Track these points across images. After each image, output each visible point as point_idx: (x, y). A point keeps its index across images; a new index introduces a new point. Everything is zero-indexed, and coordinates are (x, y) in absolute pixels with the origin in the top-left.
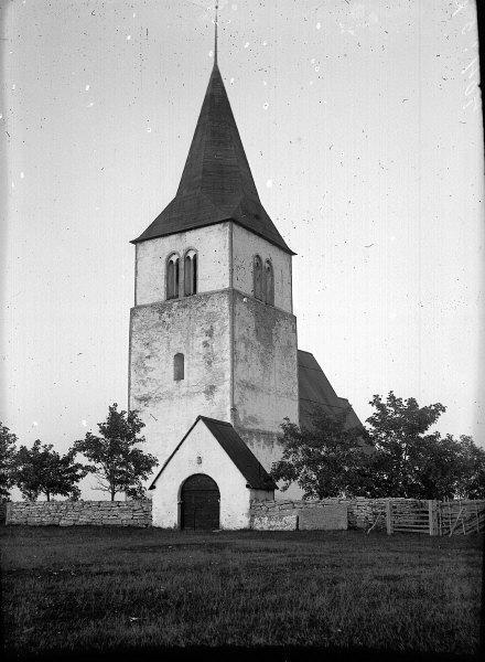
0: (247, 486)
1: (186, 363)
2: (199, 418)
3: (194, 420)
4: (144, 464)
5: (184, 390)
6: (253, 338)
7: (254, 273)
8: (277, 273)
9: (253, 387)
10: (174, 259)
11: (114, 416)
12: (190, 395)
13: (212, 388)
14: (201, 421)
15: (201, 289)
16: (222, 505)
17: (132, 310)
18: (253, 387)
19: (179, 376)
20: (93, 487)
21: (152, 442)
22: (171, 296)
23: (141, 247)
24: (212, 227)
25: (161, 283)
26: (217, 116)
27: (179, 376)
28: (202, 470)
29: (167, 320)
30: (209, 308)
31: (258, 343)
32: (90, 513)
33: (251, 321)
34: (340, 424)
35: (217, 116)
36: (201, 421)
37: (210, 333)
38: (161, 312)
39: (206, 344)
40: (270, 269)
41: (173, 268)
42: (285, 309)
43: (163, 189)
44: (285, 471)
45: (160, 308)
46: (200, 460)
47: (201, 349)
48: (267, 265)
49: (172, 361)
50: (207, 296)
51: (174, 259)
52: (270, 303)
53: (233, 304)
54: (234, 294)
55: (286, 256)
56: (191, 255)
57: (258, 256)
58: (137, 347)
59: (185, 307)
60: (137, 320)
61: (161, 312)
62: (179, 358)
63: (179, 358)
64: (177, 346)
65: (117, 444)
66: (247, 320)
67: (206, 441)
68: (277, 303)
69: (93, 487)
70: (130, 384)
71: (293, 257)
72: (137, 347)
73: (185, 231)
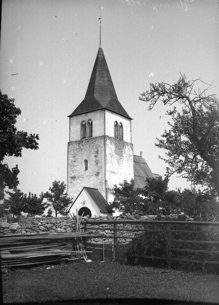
2: (84, 188)
4: (67, 202)
5: (87, 174)
6: (114, 154)
7: (115, 129)
9: (114, 173)
10: (84, 123)
11: (56, 185)
12: (90, 176)
13: (98, 173)
14: (84, 190)
15: (95, 134)
17: (68, 143)
18: (114, 173)
20: (49, 208)
21: (71, 192)
23: (71, 118)
24: (98, 111)
26: (100, 65)
27: (86, 169)
28: (85, 206)
29: (82, 147)
30: (97, 143)
31: (116, 155)
33: (113, 147)
34: (25, 198)
35: (100, 65)
37: (97, 152)
39: (96, 156)
40: (122, 126)
41: (83, 126)
43: (79, 96)
44: (115, 205)
45: (80, 142)
47: (94, 158)
51: (84, 123)
56: (90, 122)
58: (71, 158)
59: (88, 142)
60: (70, 147)
62: (86, 161)
63: (86, 161)
64: (84, 158)
65: (58, 194)
67: (85, 196)
69: (49, 208)
72: (71, 158)
73: (88, 113)
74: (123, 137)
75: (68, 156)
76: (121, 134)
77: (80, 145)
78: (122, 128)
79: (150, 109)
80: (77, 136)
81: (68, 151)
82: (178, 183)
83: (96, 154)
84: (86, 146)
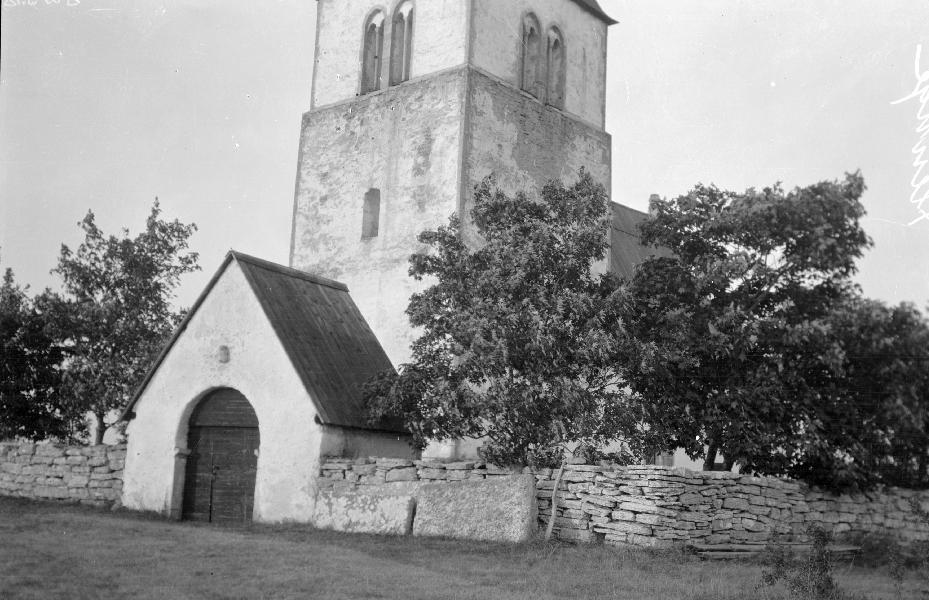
0: (317, 420)
1: (383, 206)
3: (222, 259)
6: (511, 163)
8: (572, 49)
10: (377, 21)
16: (261, 463)
17: (307, 120)
19: (371, 231)
22: (367, 85)
25: (354, 65)
27: (371, 231)
29: (359, 131)
32: (15, 468)
36: (235, 269)
38: (349, 118)
40: (558, 45)
42: (590, 117)
45: (351, 110)
46: (225, 353)
48: (553, 35)
49: (361, 202)
50: (425, 83)
51: (377, 21)
52: (552, 104)
53: (470, 92)
54: (473, 77)
55: (596, 23)
57: (532, 15)
58: (311, 181)
60: (311, 133)
61: (349, 118)
62: (373, 196)
63: (373, 196)
66: (498, 126)
67: (241, 304)
68: (572, 104)
70: (292, 247)
71: (611, 28)
72: (311, 181)
74: (561, 97)
75: (299, 176)
76: (555, 82)
77: (356, 121)
78: (563, 56)
79: (583, 167)
80: (343, 84)
81: (301, 154)
82: (426, 438)
83: (421, 160)
84: (377, 119)
